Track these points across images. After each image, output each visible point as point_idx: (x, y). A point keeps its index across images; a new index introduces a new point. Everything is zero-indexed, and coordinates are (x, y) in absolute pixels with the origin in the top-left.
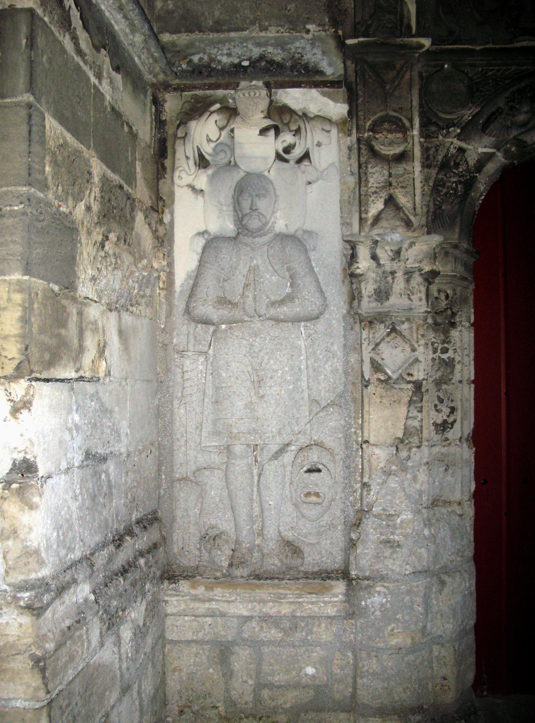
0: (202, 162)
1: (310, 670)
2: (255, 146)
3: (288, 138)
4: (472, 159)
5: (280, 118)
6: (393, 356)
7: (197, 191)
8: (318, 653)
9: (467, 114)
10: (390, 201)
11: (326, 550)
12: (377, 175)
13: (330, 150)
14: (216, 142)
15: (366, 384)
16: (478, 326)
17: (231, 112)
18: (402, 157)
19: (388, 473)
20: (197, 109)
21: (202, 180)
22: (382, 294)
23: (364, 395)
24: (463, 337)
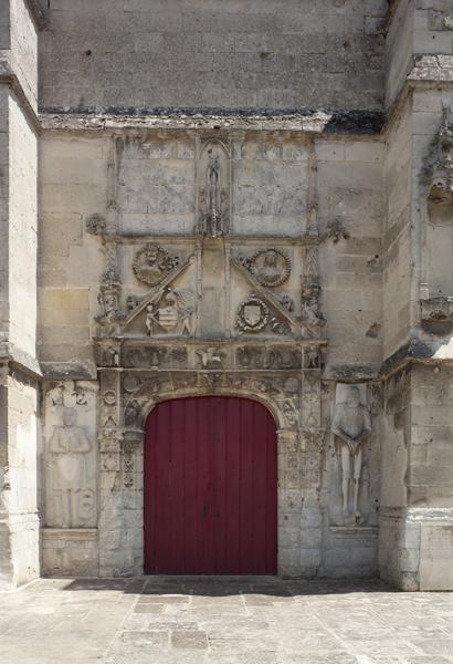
0: (54, 404)
1: (86, 556)
2: (70, 400)
3: (80, 397)
4: (140, 402)
5: (78, 390)
6: (111, 463)
7: (53, 413)
8: (89, 551)
9: (137, 389)
10: (110, 418)
11: (91, 523)
12: (106, 410)
13: (91, 398)
14: (91, 448)
15: (101, 471)
16: (146, 455)
17: (63, 388)
18: (113, 405)
19: (109, 498)
20: (53, 386)
21: (54, 409)
22: (107, 446)
23: (438, 594)
24: (138, 459)
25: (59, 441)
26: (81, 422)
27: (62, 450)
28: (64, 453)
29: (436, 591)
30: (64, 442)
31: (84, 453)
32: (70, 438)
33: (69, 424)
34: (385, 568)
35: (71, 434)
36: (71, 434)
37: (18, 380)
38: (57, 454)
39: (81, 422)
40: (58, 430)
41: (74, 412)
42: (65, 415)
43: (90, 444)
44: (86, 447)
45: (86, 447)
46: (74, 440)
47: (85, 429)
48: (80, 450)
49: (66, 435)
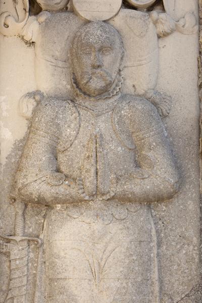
14: (181, 179)
25: (54, 154)
26: (139, 76)
27: (63, 190)
28: (75, 202)
29: (16, 10)
30: (77, 157)
31: (151, 201)
32: (98, 140)
33: (96, 84)
34: (156, 93)
35: (103, 126)
36: (103, 126)
37: (198, 235)
38: (43, 205)
39: (139, 76)
40: (48, 112)
41: (113, 42)
42: (77, 50)
43: (178, 168)
44: (159, 175)
45: (159, 175)
46: (115, 149)
47: (157, 106)
48: (138, 187)
49: (81, 128)
